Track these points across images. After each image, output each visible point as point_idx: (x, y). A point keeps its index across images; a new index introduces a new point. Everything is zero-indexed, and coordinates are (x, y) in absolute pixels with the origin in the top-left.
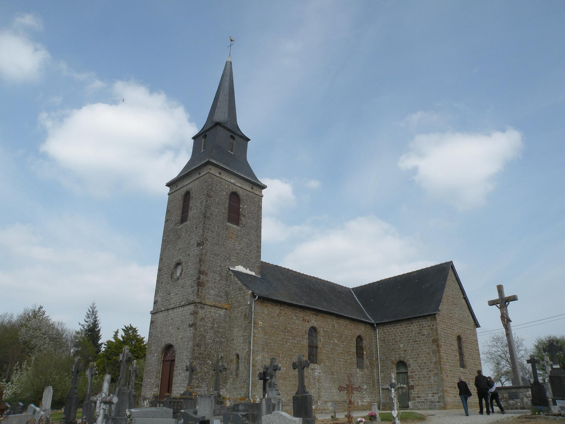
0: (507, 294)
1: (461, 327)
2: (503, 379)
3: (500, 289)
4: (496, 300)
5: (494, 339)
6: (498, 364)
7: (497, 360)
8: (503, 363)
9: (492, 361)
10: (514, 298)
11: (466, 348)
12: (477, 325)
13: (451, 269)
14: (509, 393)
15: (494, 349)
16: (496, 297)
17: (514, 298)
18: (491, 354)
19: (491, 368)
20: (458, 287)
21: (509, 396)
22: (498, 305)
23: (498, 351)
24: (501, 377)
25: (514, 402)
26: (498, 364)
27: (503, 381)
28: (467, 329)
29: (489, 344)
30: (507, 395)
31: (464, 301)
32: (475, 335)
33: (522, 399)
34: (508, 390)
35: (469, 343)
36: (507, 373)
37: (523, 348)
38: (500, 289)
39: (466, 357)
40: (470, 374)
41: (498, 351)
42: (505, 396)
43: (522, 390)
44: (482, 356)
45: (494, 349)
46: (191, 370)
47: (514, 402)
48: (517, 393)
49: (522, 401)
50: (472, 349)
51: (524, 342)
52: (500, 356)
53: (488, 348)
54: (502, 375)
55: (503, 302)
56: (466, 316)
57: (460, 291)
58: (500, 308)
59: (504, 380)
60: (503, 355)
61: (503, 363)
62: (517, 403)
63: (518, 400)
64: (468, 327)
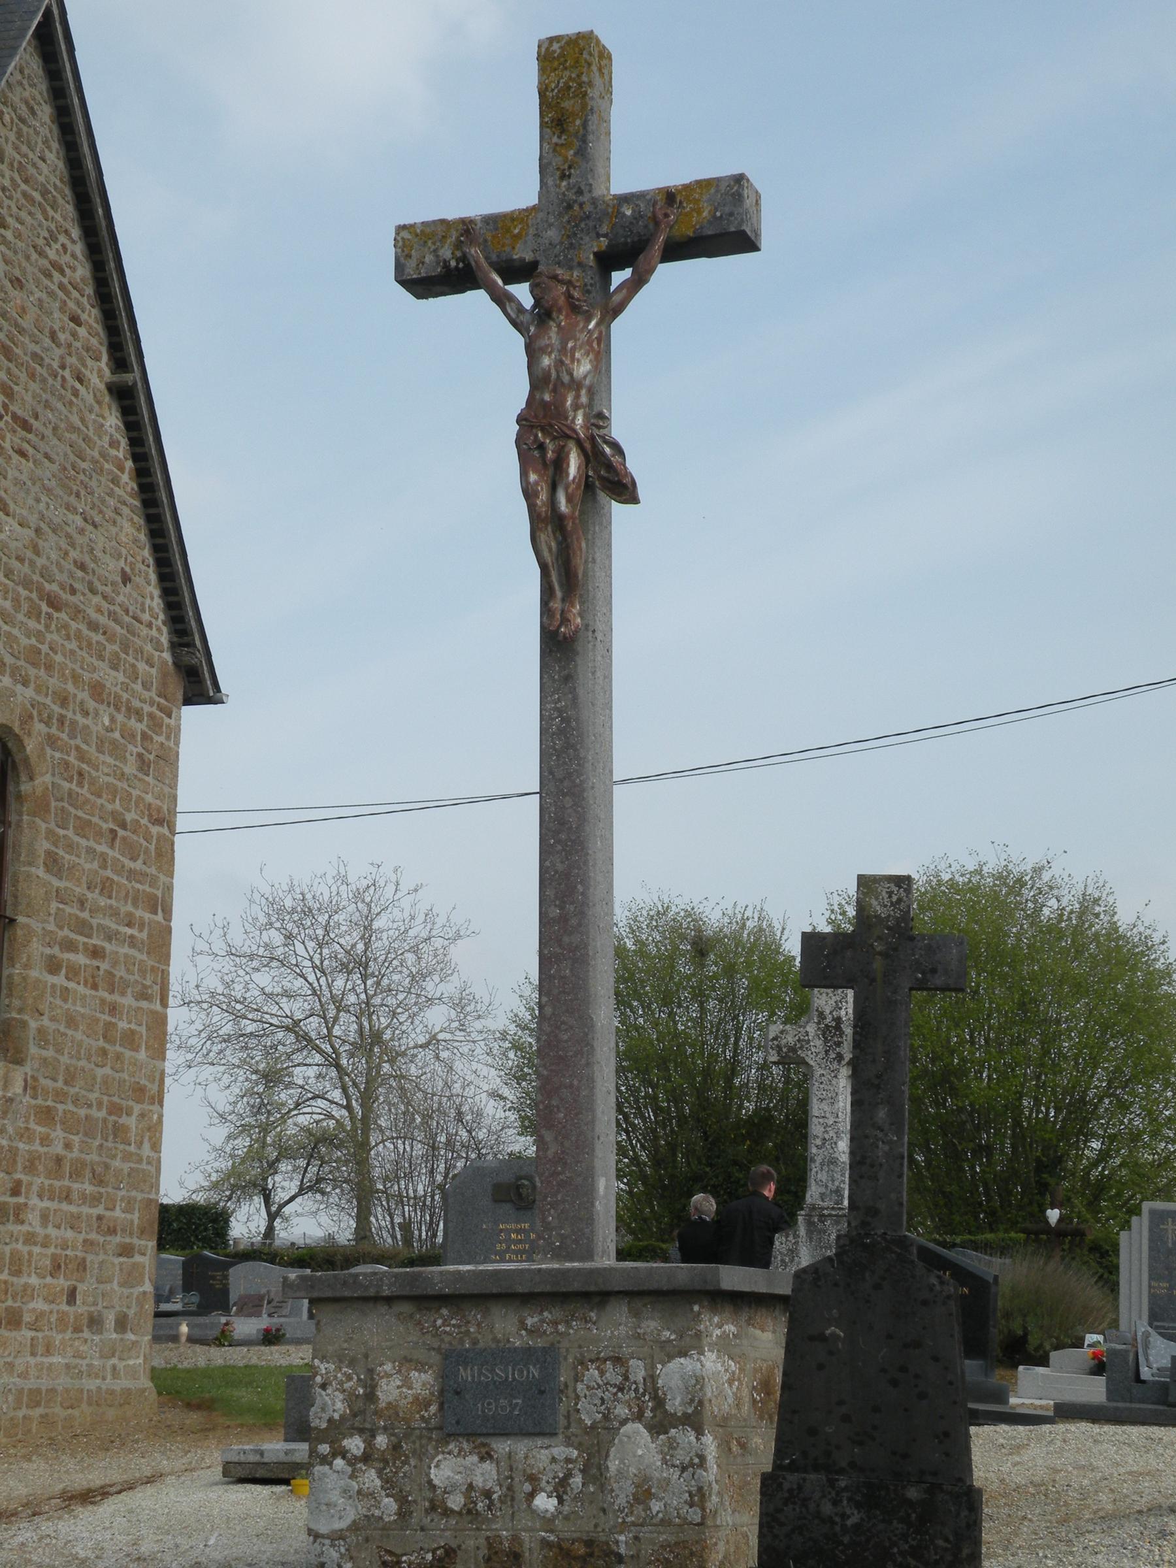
0: (640, 159)
1: (33, 656)
2: (284, 1183)
3: (571, 82)
4: (499, 223)
5: (281, 911)
6: (272, 1078)
7: (269, 1051)
8: (306, 1072)
9: (233, 1056)
10: (711, 224)
11: (53, 863)
12: (197, 683)
13: (26, 57)
14: (451, 1361)
15: (263, 979)
16: (503, 177)
17: (711, 224)
18: (235, 1008)
19: (222, 1100)
20: (82, 271)
21: (450, 1392)
22: (522, 292)
23: (288, 995)
24: (272, 1167)
25: (485, 1474)
26: (272, 1078)
27: (280, 1196)
28: (97, 690)
29: (237, 938)
30: (423, 1381)
31: (113, 421)
32: (162, 762)
33: (596, 1444)
34: (444, 1322)
35: (83, 828)
36: (316, 1144)
37: (449, 988)
38: (571, 82)
39: (37, 949)
40: (46, 1115)
41: (288, 995)
42: (389, 1390)
43: (615, 1326)
44: (177, 1018)
45: (263, 979)
46: (901, 1204)
47: (485, 1474)
48: (547, 1357)
49: (594, 1470)
50: (106, 888)
51: (457, 953)
52: (293, 1027)
53: (227, 964)
54: (285, 1153)
55: (570, 250)
56: (111, 567)
57: (91, 315)
58: (533, 325)
59: (293, 1187)
60: (313, 1026)
61: (306, 1072)
62: (518, 1486)
63: (547, 1455)
64: (113, 679)
